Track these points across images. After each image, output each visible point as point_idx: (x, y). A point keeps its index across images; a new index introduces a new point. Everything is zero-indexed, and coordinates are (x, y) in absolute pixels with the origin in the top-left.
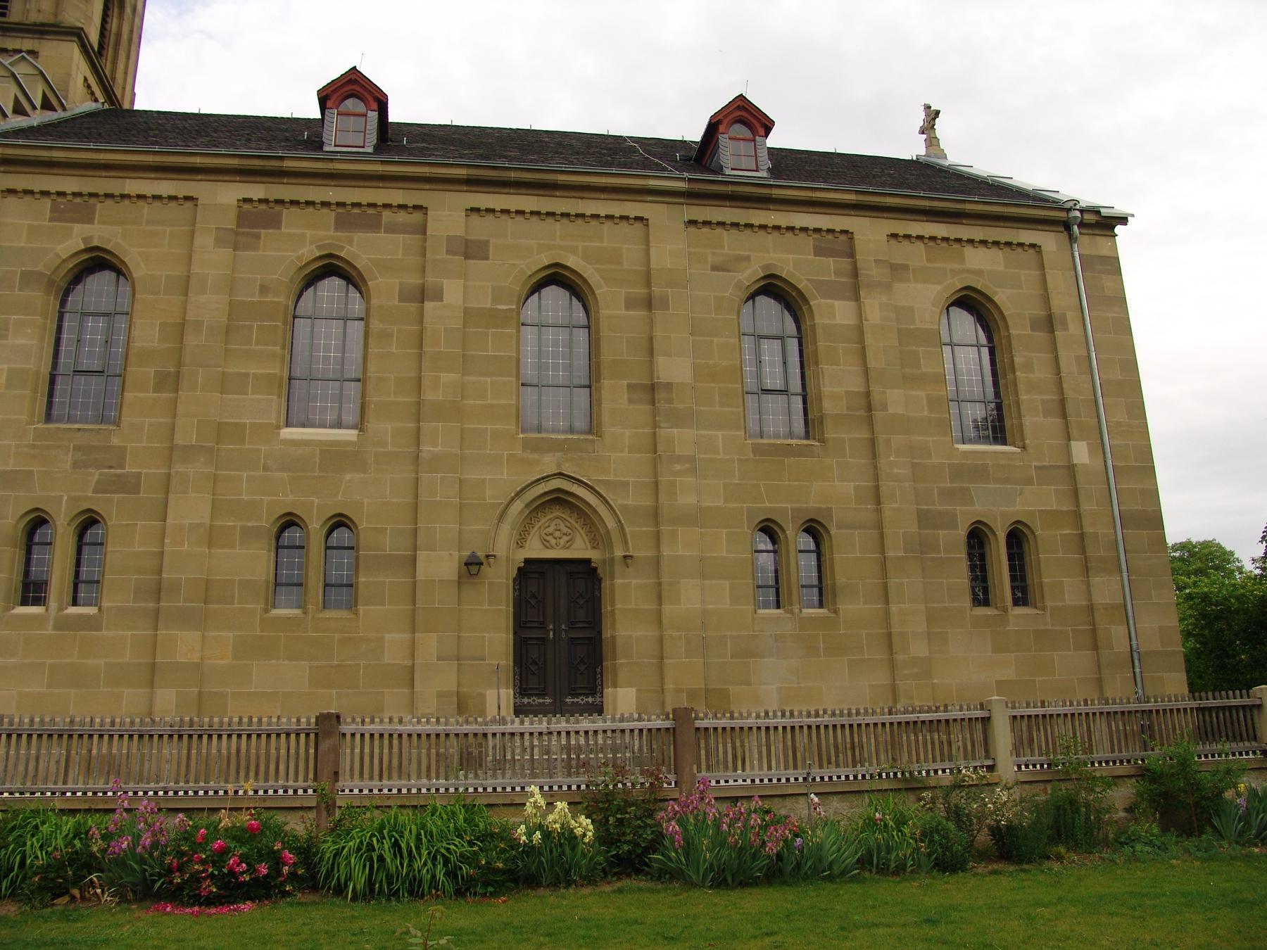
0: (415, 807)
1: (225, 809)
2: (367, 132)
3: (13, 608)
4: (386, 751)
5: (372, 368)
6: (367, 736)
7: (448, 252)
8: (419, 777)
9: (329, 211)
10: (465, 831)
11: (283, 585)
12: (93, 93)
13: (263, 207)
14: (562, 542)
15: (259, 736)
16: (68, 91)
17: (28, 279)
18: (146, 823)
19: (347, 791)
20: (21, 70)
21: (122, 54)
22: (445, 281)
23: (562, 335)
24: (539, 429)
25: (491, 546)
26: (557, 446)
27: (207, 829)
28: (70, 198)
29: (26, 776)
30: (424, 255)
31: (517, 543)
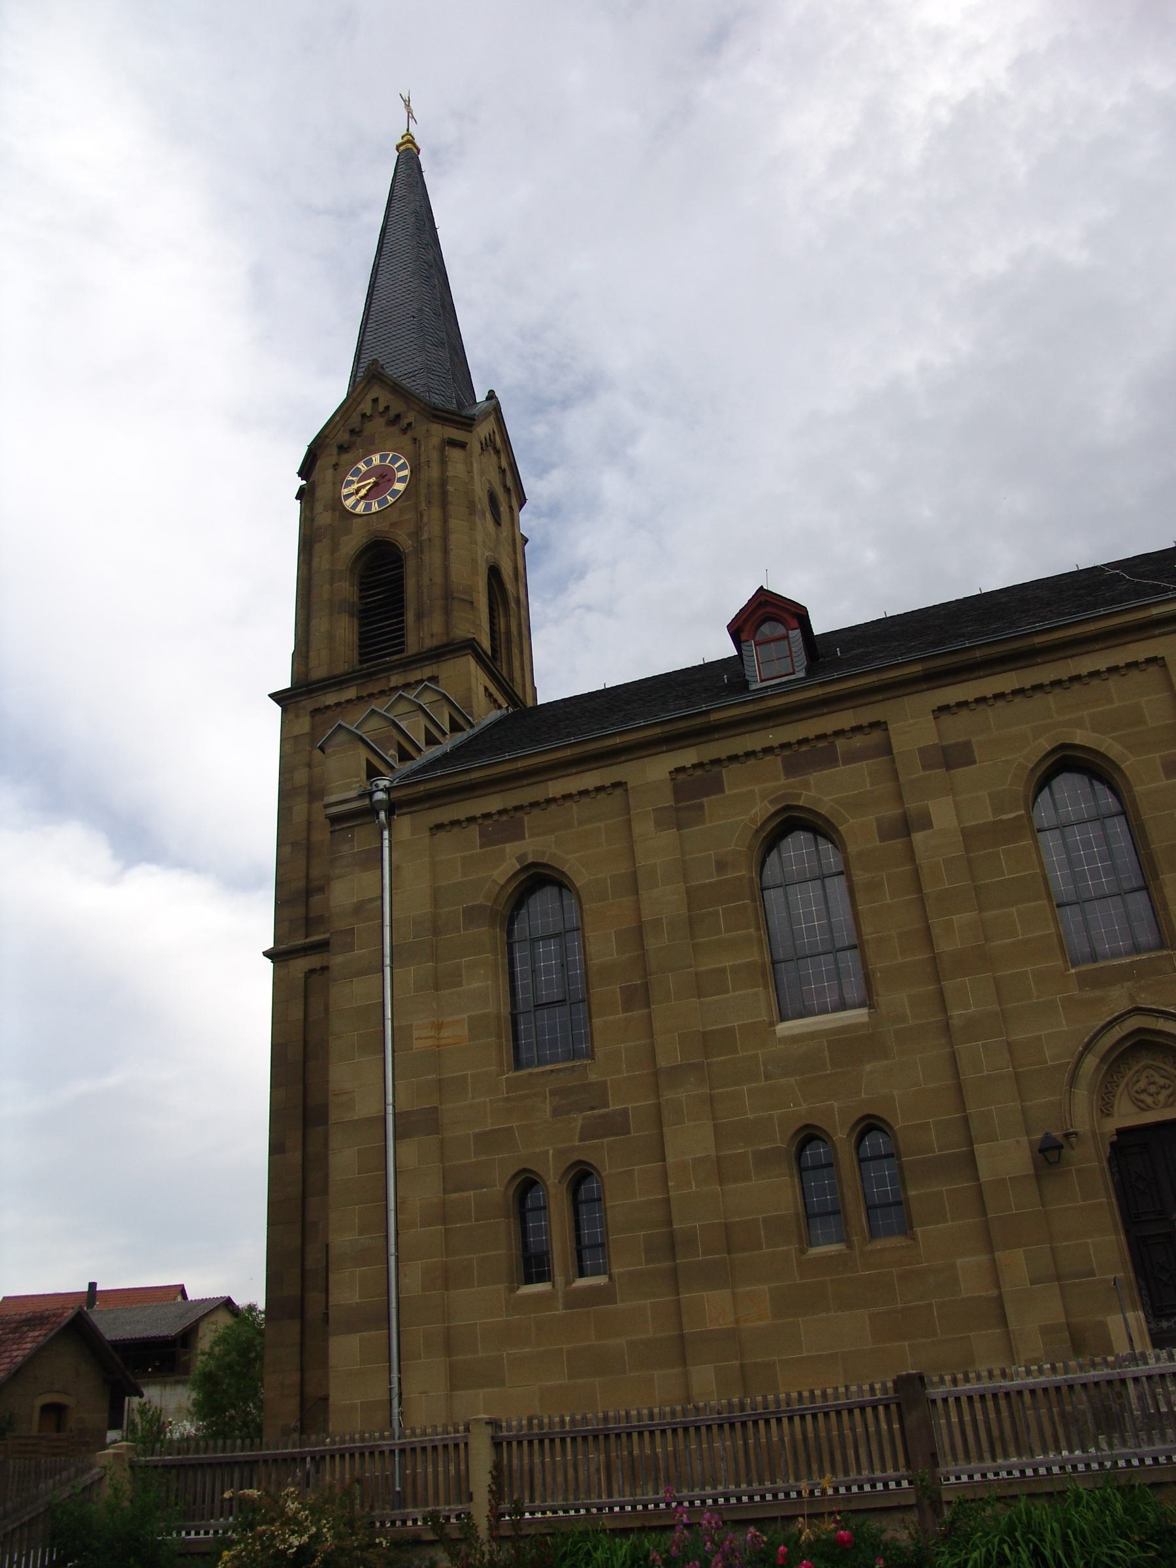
0: (1050, 1494)
1: (803, 1516)
2: (794, 655)
3: (518, 1288)
4: (992, 1415)
5: (868, 930)
6: (964, 1399)
7: (924, 768)
8: (1045, 1452)
9: (774, 757)
10: (1130, 1527)
11: (815, 1216)
12: (495, 701)
13: (699, 772)
14: (1162, 1098)
15: (826, 1414)
16: (471, 706)
17: (471, 914)
18: (713, 1542)
19: (953, 1479)
20: (425, 700)
21: (515, 651)
22: (930, 803)
23: (1092, 832)
24: (1094, 958)
25: (1068, 1122)
26: (1122, 975)
27: (786, 1545)
28: (496, 817)
29: (566, 1491)
30: (897, 779)
31: (1101, 1110)
